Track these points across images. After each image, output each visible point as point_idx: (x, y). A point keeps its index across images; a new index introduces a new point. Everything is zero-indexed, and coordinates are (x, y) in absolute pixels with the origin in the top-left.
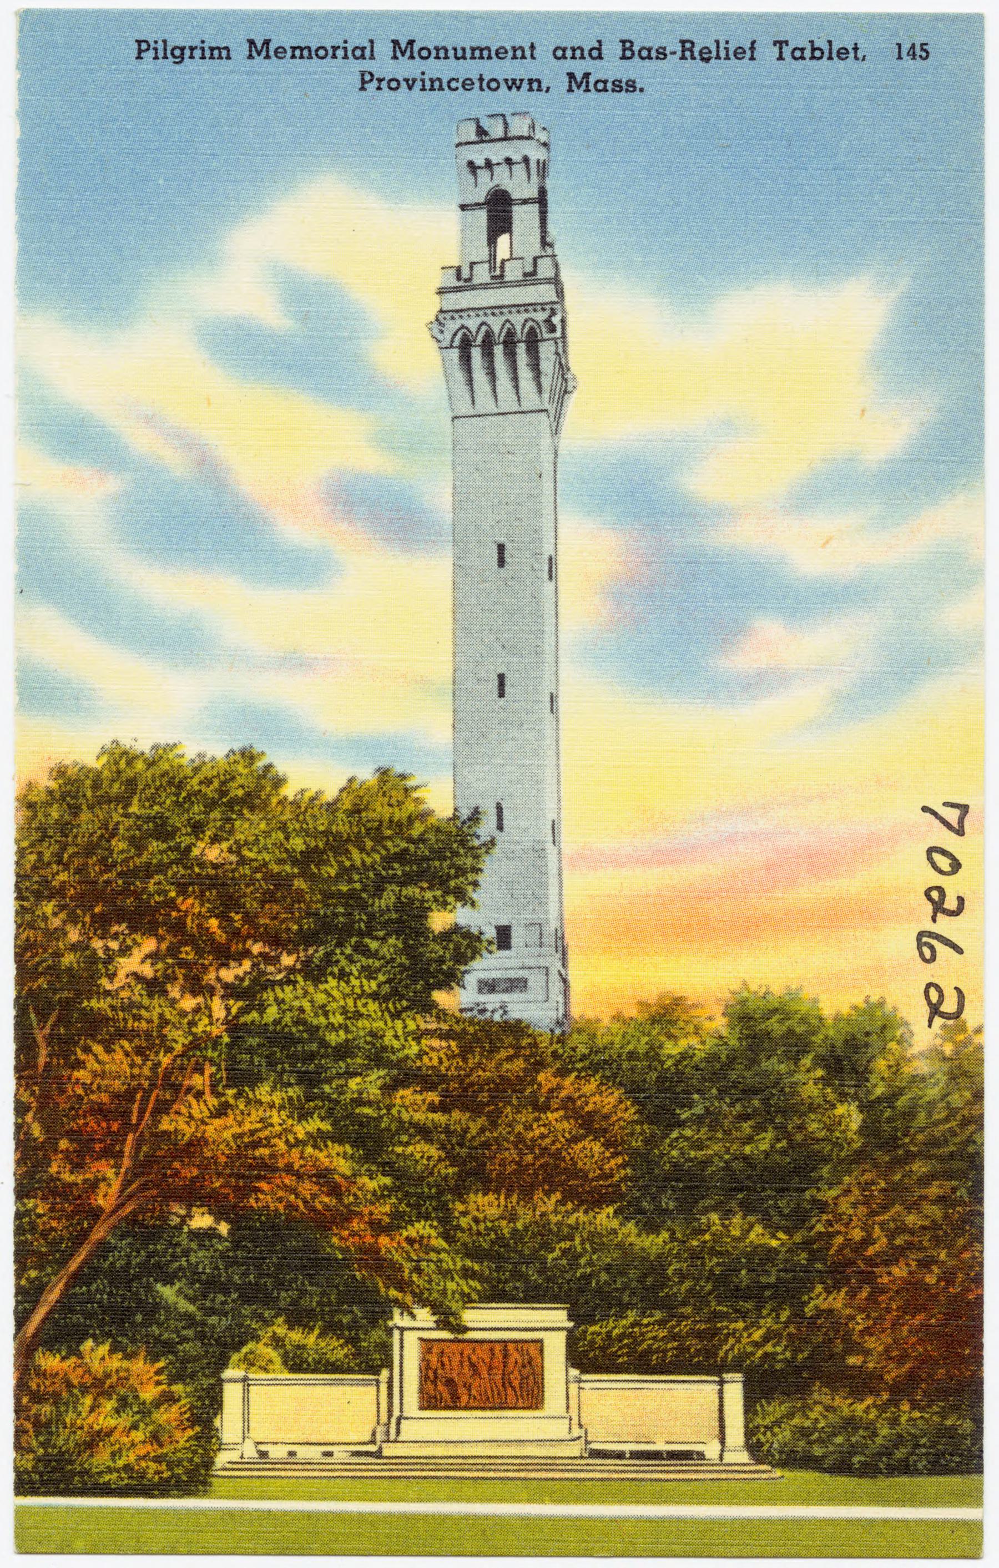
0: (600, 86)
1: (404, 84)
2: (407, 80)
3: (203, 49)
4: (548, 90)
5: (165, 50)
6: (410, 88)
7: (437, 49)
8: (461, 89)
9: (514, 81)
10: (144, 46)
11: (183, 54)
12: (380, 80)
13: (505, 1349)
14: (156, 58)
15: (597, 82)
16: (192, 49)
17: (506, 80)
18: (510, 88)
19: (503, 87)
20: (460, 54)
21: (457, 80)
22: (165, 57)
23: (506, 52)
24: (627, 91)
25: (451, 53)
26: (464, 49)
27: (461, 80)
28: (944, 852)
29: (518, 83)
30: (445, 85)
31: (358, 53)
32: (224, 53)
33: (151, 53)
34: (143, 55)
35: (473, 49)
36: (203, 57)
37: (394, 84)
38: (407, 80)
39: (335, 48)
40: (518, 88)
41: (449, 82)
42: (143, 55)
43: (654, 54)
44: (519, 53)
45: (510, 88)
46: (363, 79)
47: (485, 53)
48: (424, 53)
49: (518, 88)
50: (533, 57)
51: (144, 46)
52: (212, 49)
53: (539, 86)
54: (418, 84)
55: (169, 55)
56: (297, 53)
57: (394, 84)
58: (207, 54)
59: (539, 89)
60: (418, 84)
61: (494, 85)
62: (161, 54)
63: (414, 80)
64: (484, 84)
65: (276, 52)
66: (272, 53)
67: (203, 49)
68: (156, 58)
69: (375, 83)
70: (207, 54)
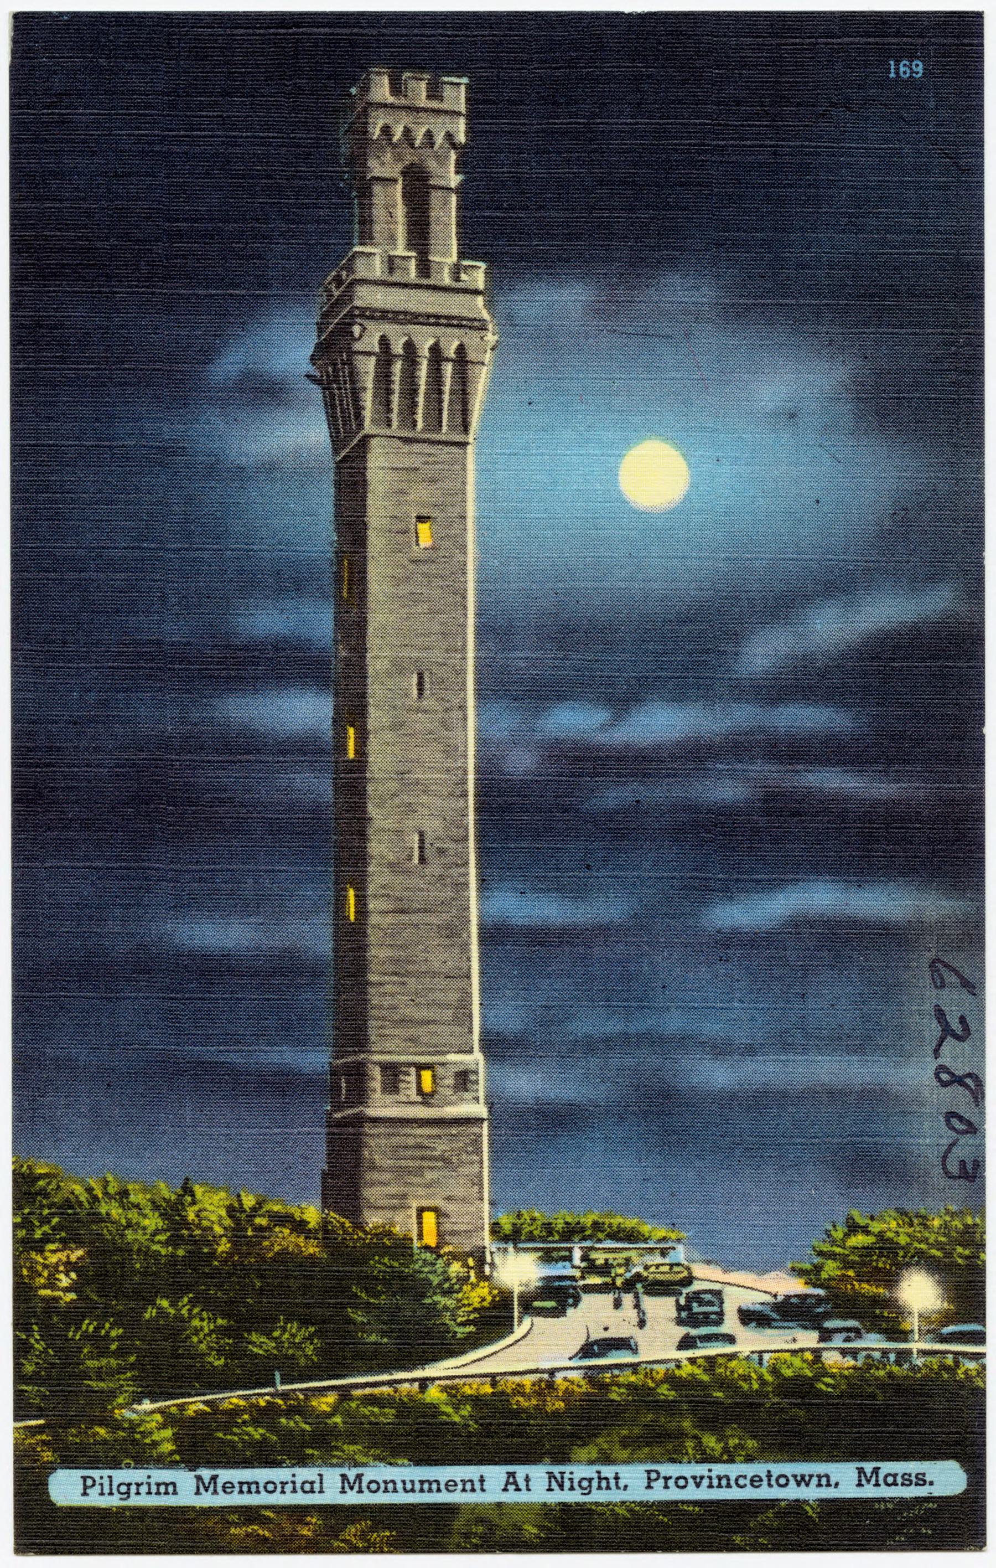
0: (890, 1480)
1: (691, 1481)
2: (694, 1478)
3: (149, 1484)
4: (837, 1484)
5: (111, 1485)
6: (698, 1485)
7: (385, 1482)
8: (749, 1486)
9: (803, 1477)
10: (89, 1482)
11: (590, 1486)
12: (667, 1479)
13: (425, 268)
14: (102, 1494)
15: (886, 1476)
16: (138, 1485)
17: (795, 1476)
18: (799, 1484)
19: (792, 1482)
20: (409, 1486)
21: (745, 1477)
22: (111, 1494)
23: (456, 1485)
24: (917, 1484)
25: (400, 1486)
26: (412, 1482)
27: (749, 1478)
28: (961, 1118)
29: (807, 1478)
30: (732, 1482)
31: (307, 1487)
32: (171, 1489)
33: (98, 1488)
34: (88, 1491)
35: (422, 1482)
36: (149, 1493)
37: (682, 1482)
38: (694, 1478)
39: (284, 1484)
40: (807, 1485)
41: (737, 1480)
42: (88, 1491)
43: (899, 1480)
44: (468, 1486)
45: (799, 1484)
46: (649, 1478)
47: (434, 1486)
48: (374, 1486)
49: (807, 1485)
50: (529, 1490)
51: (89, 1482)
52: (158, 1485)
53: (828, 1481)
54: (705, 1482)
55: (115, 1491)
56: (245, 1488)
57: (682, 1482)
58: (715, 1482)
59: (828, 1485)
60: (705, 1482)
61: (782, 1481)
62: (106, 1490)
63: (702, 1478)
64: (773, 1479)
65: (224, 1487)
66: (219, 1489)
67: (149, 1484)
68: (102, 1494)
69: (661, 1481)
70: (715, 1482)
